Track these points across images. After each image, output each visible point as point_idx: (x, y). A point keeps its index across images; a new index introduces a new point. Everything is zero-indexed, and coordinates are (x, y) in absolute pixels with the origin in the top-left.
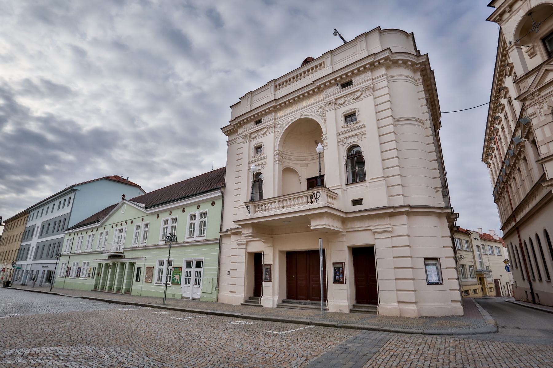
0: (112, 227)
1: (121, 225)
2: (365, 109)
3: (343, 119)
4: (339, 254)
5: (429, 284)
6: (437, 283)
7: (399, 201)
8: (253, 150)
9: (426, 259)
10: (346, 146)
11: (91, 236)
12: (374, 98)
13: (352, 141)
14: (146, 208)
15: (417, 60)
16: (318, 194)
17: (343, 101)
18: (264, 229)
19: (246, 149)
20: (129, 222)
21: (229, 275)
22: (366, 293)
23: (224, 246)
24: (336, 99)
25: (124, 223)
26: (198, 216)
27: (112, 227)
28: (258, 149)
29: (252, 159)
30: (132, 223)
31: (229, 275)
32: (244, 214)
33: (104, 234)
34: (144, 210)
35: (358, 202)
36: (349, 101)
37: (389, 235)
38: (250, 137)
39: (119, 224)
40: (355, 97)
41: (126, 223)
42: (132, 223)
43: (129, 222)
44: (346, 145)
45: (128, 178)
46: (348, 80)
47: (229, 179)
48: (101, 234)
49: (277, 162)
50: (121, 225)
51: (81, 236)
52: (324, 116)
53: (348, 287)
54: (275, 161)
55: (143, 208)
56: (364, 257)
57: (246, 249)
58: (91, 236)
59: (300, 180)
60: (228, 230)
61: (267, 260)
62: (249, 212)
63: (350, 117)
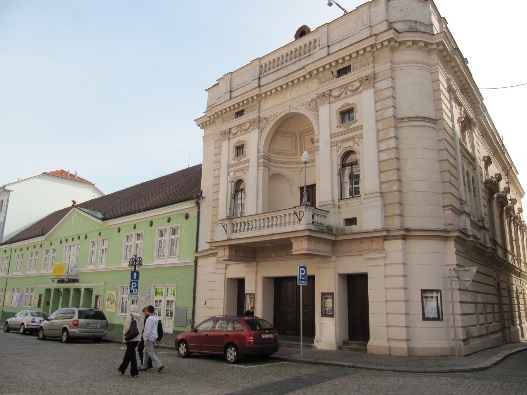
0: (61, 242)
1: (73, 240)
2: (365, 103)
3: (339, 115)
4: (327, 282)
5: (425, 318)
6: (434, 319)
7: (396, 223)
8: (232, 150)
9: (423, 291)
10: (341, 151)
11: (34, 254)
12: (375, 92)
13: (348, 145)
14: (103, 219)
15: (432, 40)
16: (302, 214)
17: (339, 93)
18: (247, 252)
19: (227, 148)
20: (83, 237)
21: (205, 304)
22: (358, 326)
23: (471, 305)
24: (331, 91)
25: (76, 238)
26: (169, 231)
27: (61, 242)
28: (240, 149)
29: (232, 162)
30: (86, 237)
31: (205, 304)
32: (221, 235)
33: (51, 251)
34: (100, 221)
35: (351, 221)
36: (346, 94)
37: (382, 262)
38: (230, 132)
39: (70, 239)
40: (354, 88)
41: (79, 237)
42: (86, 237)
43: (83, 237)
44: (341, 150)
45: (76, 173)
46: (346, 65)
47: (206, 185)
48: (47, 251)
49: (262, 168)
50: (73, 240)
51: (20, 253)
52: (316, 110)
53: (337, 320)
54: (258, 167)
55: (100, 219)
56: (356, 286)
57: (225, 274)
58: (34, 254)
59: (291, 189)
60: (204, 251)
61: (249, 288)
62: (226, 231)
63: (346, 114)
